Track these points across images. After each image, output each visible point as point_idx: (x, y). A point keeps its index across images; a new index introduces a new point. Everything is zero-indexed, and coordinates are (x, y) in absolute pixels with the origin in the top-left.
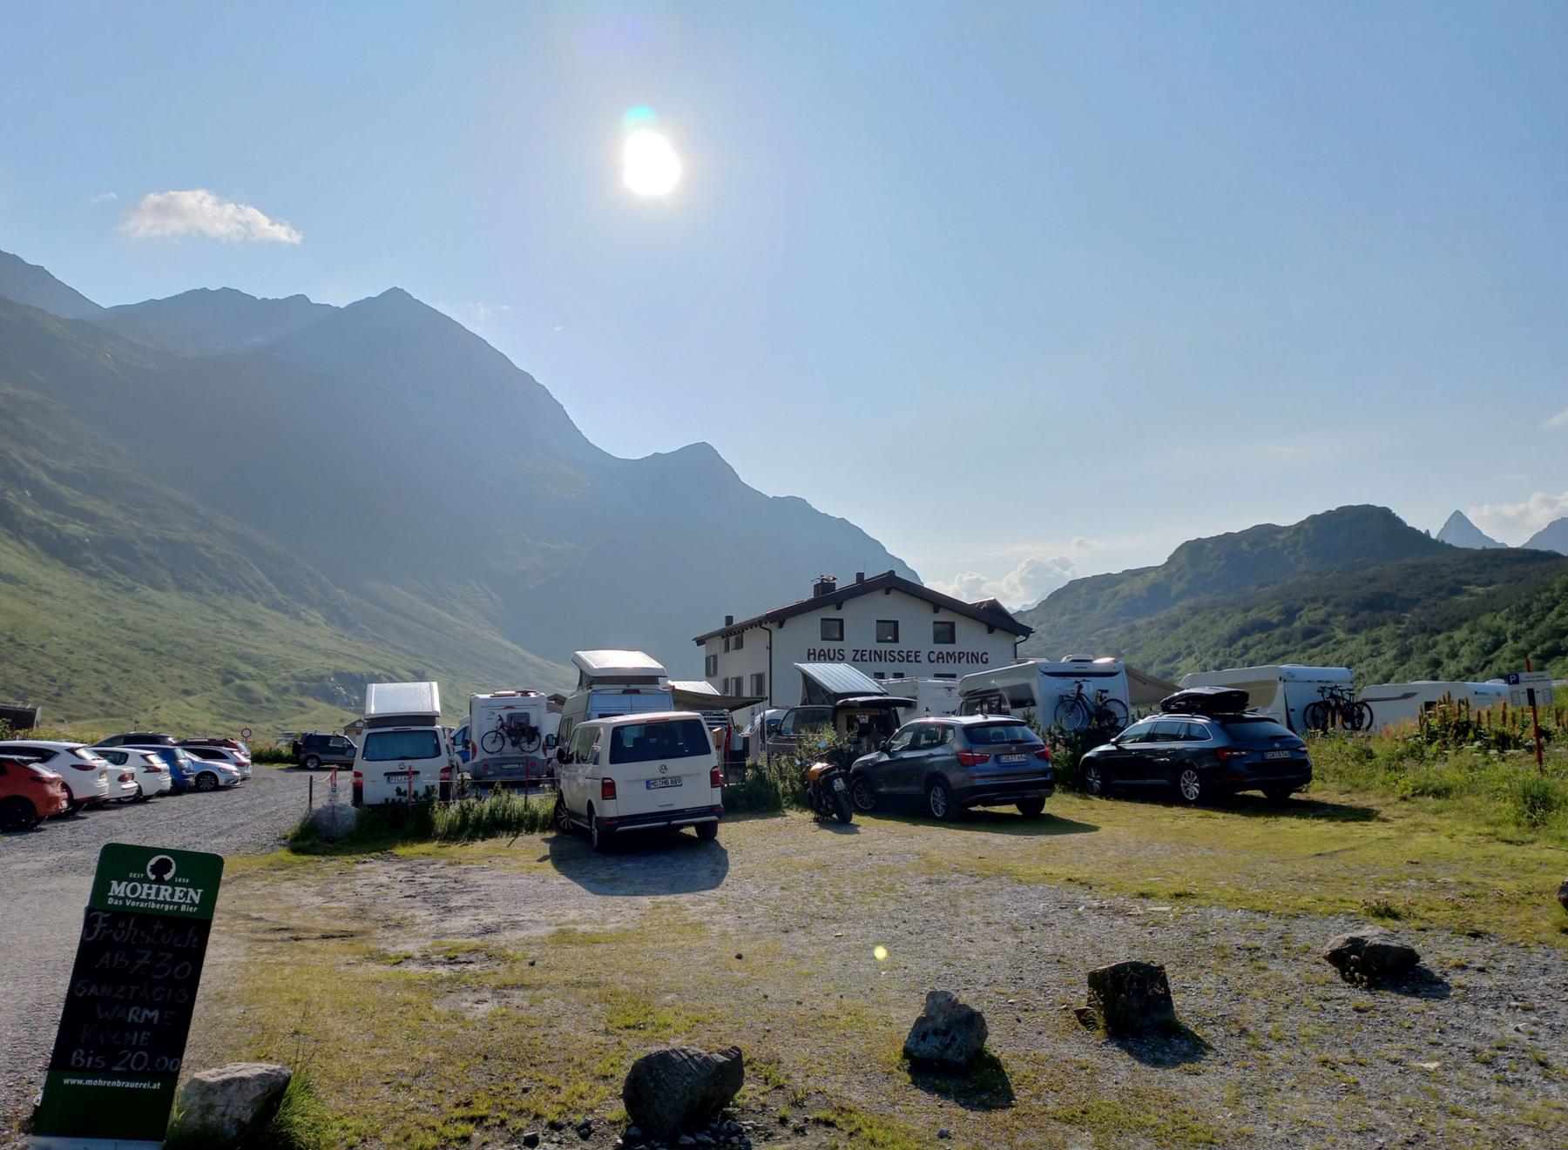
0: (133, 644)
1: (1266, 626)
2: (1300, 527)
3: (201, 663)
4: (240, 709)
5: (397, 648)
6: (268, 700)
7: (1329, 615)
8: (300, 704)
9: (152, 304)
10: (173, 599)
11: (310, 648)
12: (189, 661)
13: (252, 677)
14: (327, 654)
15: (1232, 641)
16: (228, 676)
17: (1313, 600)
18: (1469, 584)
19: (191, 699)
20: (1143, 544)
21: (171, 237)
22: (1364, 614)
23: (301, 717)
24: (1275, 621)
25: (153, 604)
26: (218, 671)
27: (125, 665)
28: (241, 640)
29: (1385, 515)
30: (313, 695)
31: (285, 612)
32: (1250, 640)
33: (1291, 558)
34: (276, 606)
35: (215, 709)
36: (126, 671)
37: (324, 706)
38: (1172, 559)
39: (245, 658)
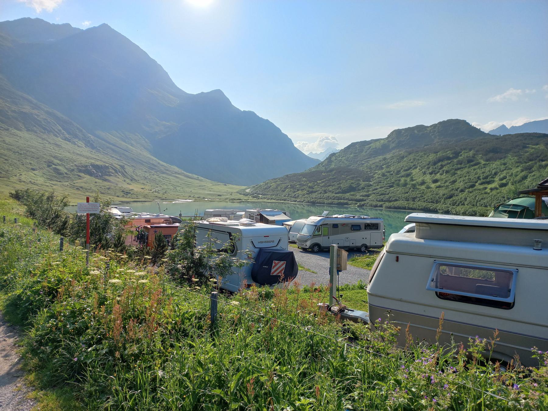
0: (9, 150)
1: (448, 158)
2: (434, 126)
3: (38, 158)
4: (55, 177)
5: (113, 157)
6: (66, 173)
7: (474, 155)
8: (79, 176)
9: (8, 22)
10: (25, 134)
11: (80, 155)
12: (33, 158)
13: (59, 164)
14: (88, 158)
15: (435, 163)
16: (50, 164)
17: (464, 149)
18: (529, 144)
19: (34, 172)
20: (381, 132)
21: (11, 16)
22: (491, 155)
23: (80, 181)
24: (451, 156)
25: (17, 136)
26: (45, 162)
27: (6, 158)
28: (53, 150)
29: (464, 123)
30: (84, 173)
31: (70, 142)
32: (444, 163)
33: (433, 137)
34: (66, 139)
35: (45, 176)
36: (6, 160)
37: (88, 177)
38: (389, 136)
39: (55, 157)
